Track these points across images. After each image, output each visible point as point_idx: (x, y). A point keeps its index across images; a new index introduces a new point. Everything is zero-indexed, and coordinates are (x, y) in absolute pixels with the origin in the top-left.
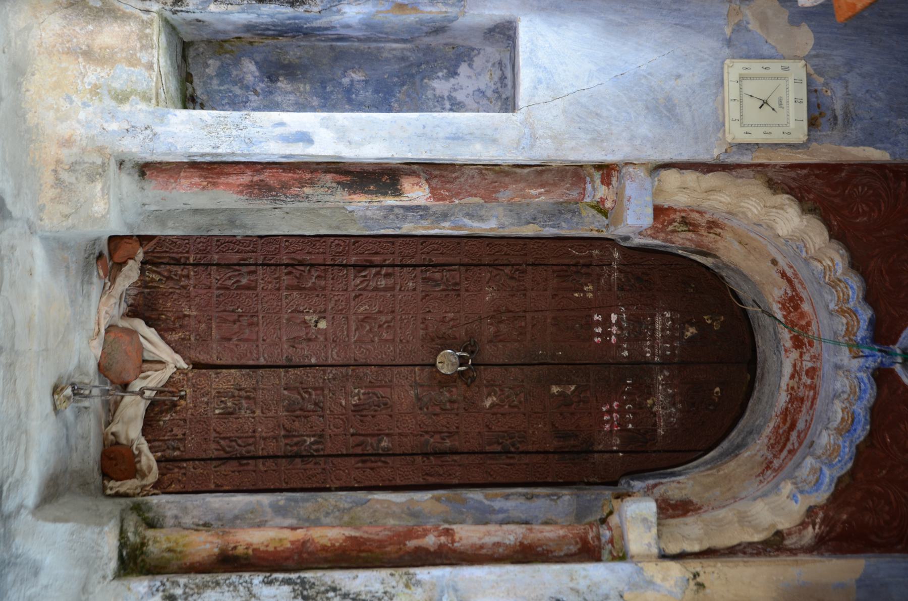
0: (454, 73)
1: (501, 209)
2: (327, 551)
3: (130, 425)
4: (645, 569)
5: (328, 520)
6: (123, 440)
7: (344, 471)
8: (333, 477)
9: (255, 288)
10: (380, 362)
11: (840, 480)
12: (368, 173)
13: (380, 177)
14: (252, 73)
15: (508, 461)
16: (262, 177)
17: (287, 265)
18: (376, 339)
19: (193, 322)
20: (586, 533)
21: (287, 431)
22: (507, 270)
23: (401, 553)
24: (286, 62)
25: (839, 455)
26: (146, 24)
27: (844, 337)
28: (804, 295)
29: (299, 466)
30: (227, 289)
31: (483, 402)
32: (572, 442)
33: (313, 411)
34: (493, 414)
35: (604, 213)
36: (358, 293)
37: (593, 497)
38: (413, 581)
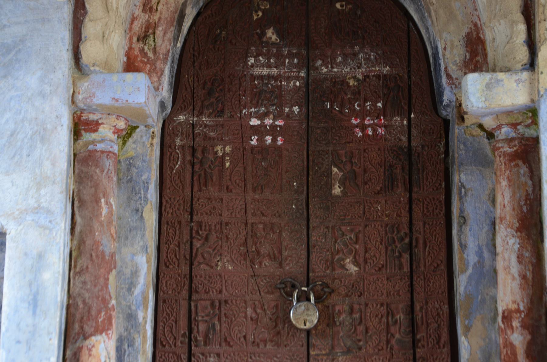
20: (505, 154)
22: (197, 244)
32: (399, 171)
34: (366, 262)
35: (132, 129)
37: (462, 147)
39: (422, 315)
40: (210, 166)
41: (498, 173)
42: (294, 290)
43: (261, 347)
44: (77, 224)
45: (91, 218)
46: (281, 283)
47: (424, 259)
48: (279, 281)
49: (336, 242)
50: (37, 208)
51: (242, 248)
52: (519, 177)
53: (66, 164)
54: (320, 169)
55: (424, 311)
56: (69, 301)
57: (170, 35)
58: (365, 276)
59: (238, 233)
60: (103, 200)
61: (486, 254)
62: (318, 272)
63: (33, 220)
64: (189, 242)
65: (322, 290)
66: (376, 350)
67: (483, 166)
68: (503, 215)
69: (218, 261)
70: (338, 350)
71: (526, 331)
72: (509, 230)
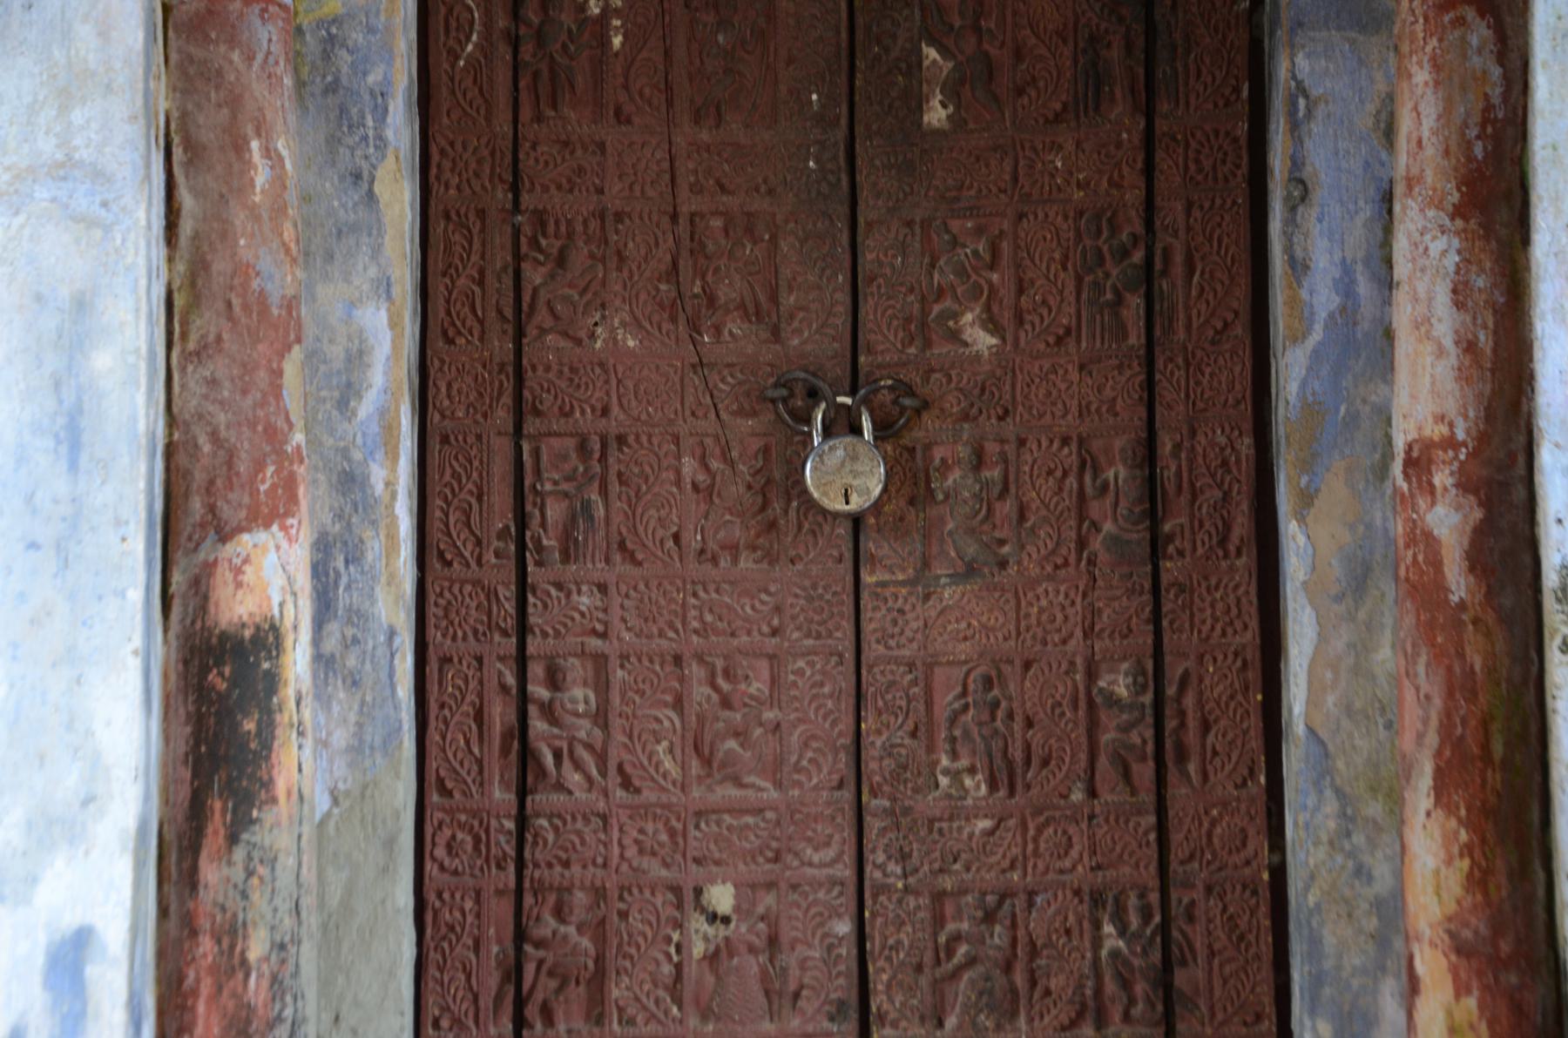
1: (323, 291)
2: (1487, 873)
7: (1213, 823)
8: (1237, 859)
10: (848, 703)
12: (197, 738)
15: (1178, 269)
18: (769, 715)
21: (1081, 1014)
22: (534, 276)
23: (1490, 618)
29: (1200, 975)
31: (978, 357)
32: (1115, 53)
33: (1014, 925)
34: (1020, 320)
36: (614, 779)
39: (1180, 467)
40: (564, 46)
41: (1405, 48)
42: (817, 404)
43: (722, 564)
44: (184, 213)
45: (222, 196)
46: (776, 386)
47: (1187, 308)
48: (771, 381)
49: (933, 266)
50: (62, 165)
51: (663, 287)
52: (1465, 56)
53: (141, 35)
54: (887, 50)
55: (1183, 455)
56: (171, 435)
58: (1018, 360)
59: (652, 242)
60: (255, 145)
61: (1364, 287)
62: (882, 352)
63: (54, 200)
64: (510, 270)
65: (895, 402)
66: (1049, 569)
67: (1363, 29)
68: (1415, 171)
69: (596, 324)
70: (940, 570)
71: (1472, 498)
72: (1431, 213)
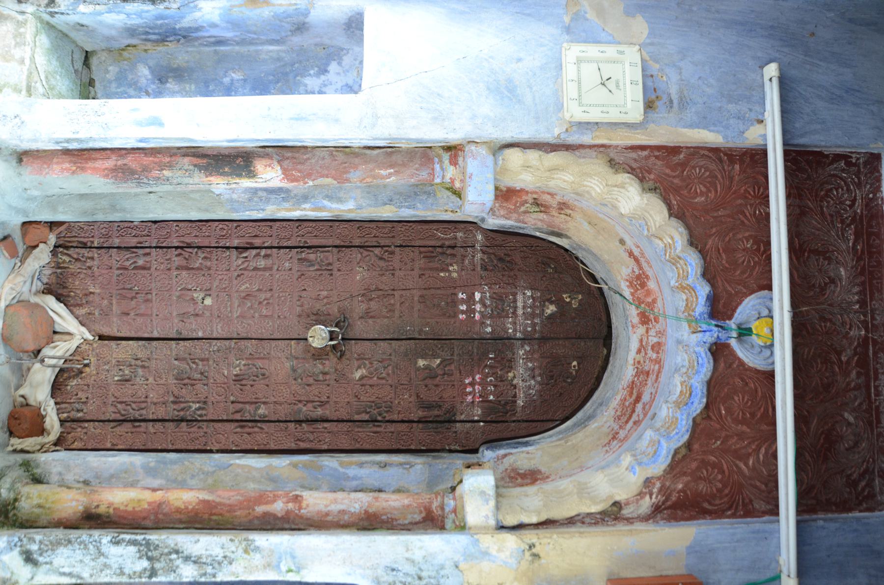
0: (324, 71)
2: (180, 513)
3: (38, 388)
4: (481, 541)
5: (193, 482)
6: (32, 402)
8: (213, 441)
9: (149, 269)
11: (676, 452)
13: (235, 160)
14: (145, 76)
15: (375, 429)
16: (125, 161)
17: (177, 248)
18: (257, 315)
19: (97, 299)
20: (431, 503)
22: (377, 251)
23: (250, 517)
24: (175, 66)
25: (676, 428)
26: (21, 24)
27: (684, 312)
28: (650, 273)
30: (126, 269)
31: (352, 373)
32: (436, 412)
37: (445, 466)
38: (252, 547)
57: (540, 224)
67: (428, 483)
